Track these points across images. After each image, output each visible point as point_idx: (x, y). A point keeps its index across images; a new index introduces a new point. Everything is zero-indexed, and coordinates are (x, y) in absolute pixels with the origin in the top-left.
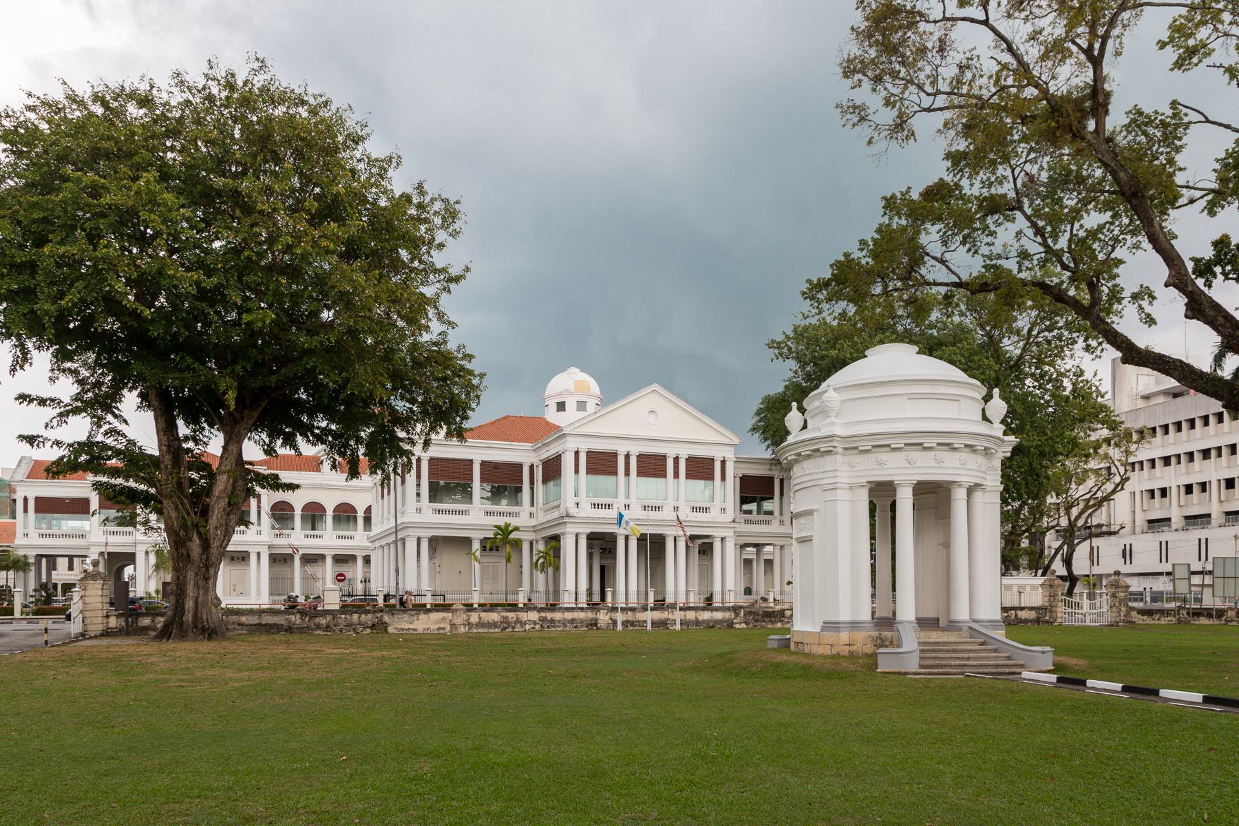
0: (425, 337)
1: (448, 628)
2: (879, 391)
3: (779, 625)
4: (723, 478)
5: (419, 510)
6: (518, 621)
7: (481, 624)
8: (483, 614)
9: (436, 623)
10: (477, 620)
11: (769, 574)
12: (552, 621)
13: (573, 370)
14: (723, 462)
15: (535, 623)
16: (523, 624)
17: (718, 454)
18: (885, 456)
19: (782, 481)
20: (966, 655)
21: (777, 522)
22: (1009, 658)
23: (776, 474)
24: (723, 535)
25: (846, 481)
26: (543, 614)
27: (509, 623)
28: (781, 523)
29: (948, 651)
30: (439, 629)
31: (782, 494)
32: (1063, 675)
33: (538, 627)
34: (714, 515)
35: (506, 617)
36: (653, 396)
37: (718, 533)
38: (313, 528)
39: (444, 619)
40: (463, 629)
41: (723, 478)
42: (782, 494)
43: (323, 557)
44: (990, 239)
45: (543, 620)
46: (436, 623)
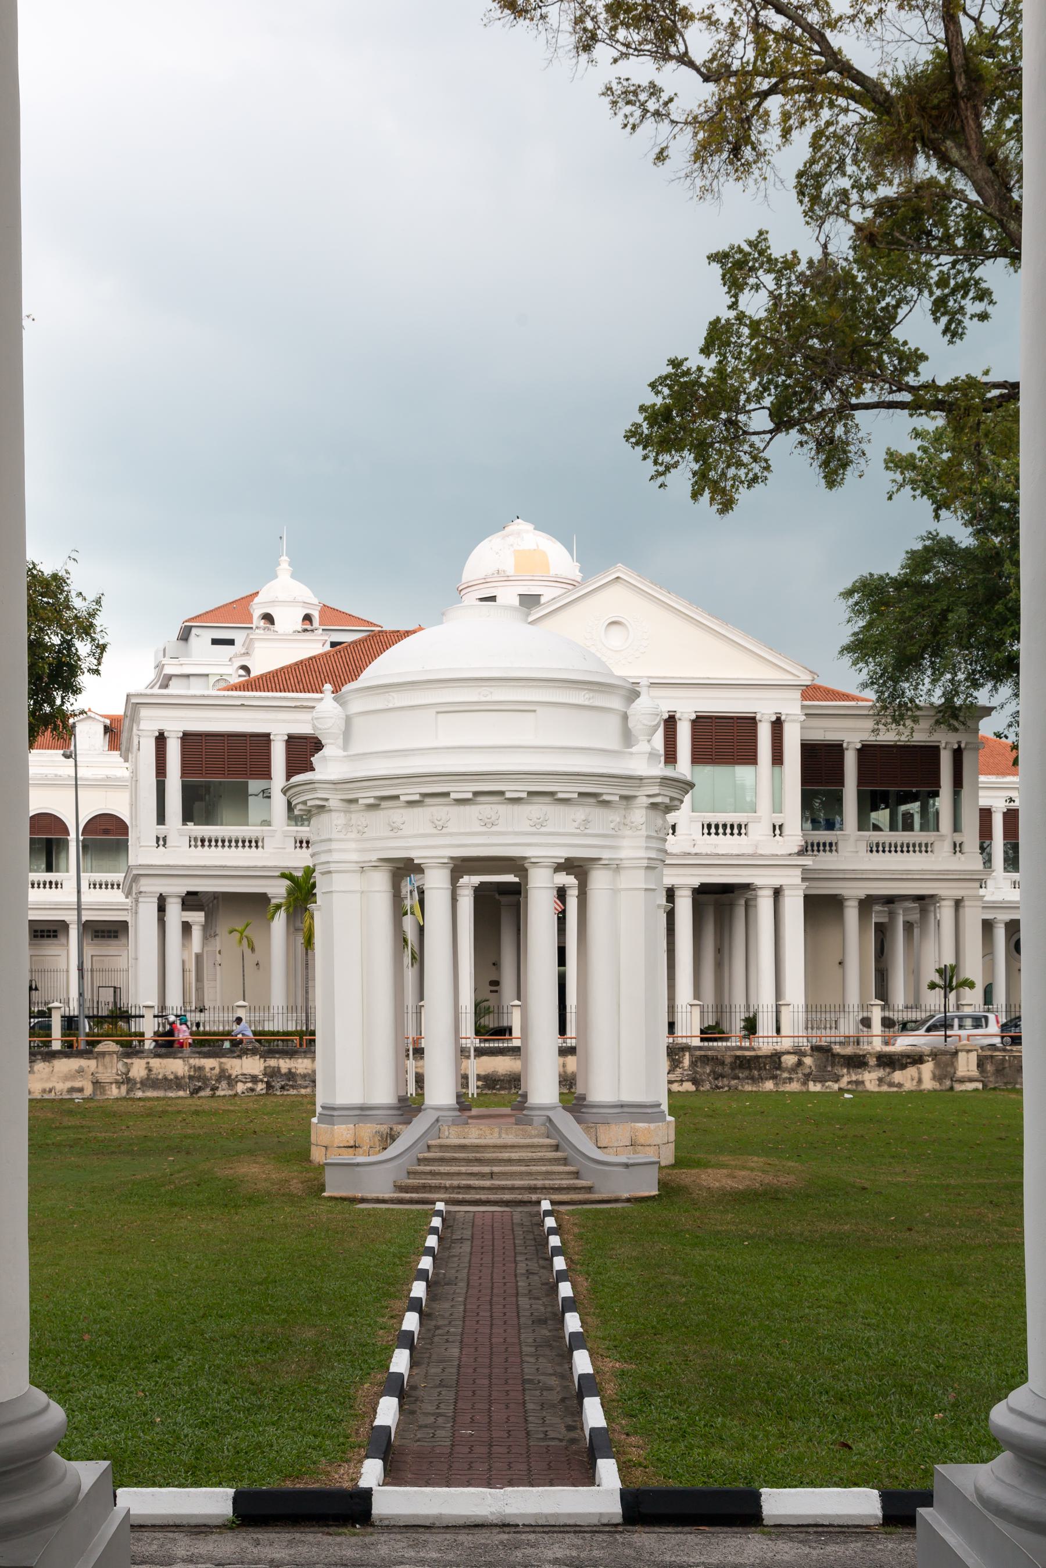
0: (865, 274)
1: (89, 1091)
2: (398, 699)
3: (769, 1085)
4: (778, 759)
5: (162, 841)
6: (224, 1076)
7: (151, 1082)
8: (155, 1062)
9: (66, 1078)
10: (143, 1073)
11: (988, 957)
12: (291, 1075)
13: (521, 526)
14: (777, 725)
15: (254, 1079)
16: (231, 1081)
17: (763, 708)
18: (397, 815)
19: (958, 755)
20: (486, 1169)
21: (947, 846)
22: (576, 1175)
23: (946, 740)
24: (776, 882)
25: (354, 857)
26: (272, 1062)
27: (205, 1080)
28: (957, 848)
29: (469, 1161)
30: (72, 1090)
31: (958, 782)
32: (533, 1209)
33: (260, 1087)
34: (757, 839)
35: (201, 1069)
36: (617, 590)
37: (764, 880)
38: (49, 869)
39: (81, 1071)
40: (114, 1092)
41: (778, 759)
42: (958, 782)
43: (64, 926)
44: (979, 307)
45: (272, 1073)
46: (66, 1078)
